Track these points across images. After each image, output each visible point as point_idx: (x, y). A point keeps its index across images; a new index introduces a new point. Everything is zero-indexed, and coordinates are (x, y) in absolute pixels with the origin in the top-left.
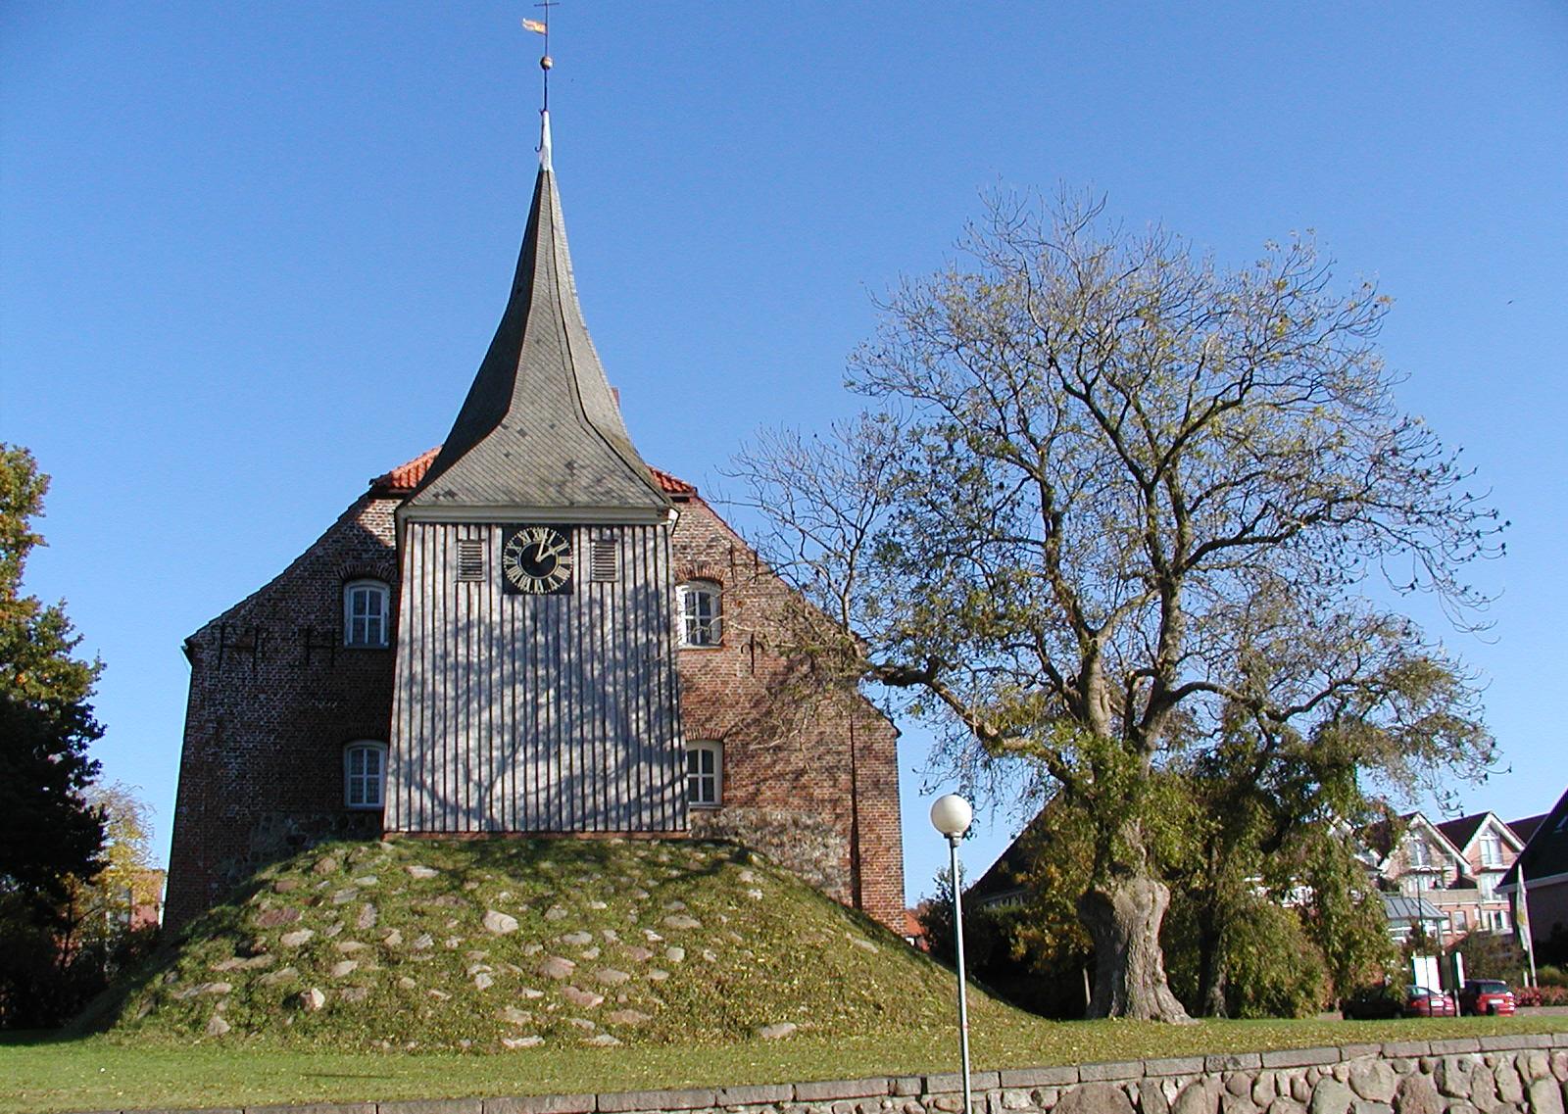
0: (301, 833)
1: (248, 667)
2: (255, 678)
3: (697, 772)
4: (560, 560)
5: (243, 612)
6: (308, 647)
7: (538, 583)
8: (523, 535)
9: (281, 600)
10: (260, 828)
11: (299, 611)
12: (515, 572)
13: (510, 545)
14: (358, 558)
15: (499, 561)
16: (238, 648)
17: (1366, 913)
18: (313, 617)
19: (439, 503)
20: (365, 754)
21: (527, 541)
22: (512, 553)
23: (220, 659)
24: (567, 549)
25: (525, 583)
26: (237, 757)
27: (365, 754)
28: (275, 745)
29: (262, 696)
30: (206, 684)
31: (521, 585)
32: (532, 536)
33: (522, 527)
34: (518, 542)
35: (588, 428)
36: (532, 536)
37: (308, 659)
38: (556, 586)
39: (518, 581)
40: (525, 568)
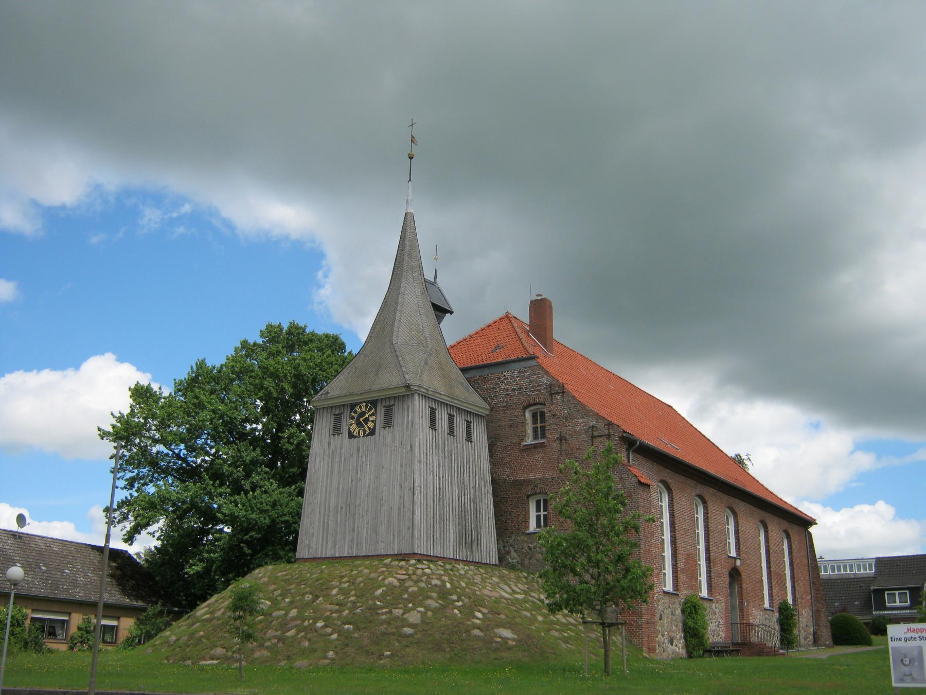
7: (361, 431)
13: (353, 414)
20: (542, 524)
21: (359, 411)
22: (352, 418)
27: (542, 524)
33: (356, 404)
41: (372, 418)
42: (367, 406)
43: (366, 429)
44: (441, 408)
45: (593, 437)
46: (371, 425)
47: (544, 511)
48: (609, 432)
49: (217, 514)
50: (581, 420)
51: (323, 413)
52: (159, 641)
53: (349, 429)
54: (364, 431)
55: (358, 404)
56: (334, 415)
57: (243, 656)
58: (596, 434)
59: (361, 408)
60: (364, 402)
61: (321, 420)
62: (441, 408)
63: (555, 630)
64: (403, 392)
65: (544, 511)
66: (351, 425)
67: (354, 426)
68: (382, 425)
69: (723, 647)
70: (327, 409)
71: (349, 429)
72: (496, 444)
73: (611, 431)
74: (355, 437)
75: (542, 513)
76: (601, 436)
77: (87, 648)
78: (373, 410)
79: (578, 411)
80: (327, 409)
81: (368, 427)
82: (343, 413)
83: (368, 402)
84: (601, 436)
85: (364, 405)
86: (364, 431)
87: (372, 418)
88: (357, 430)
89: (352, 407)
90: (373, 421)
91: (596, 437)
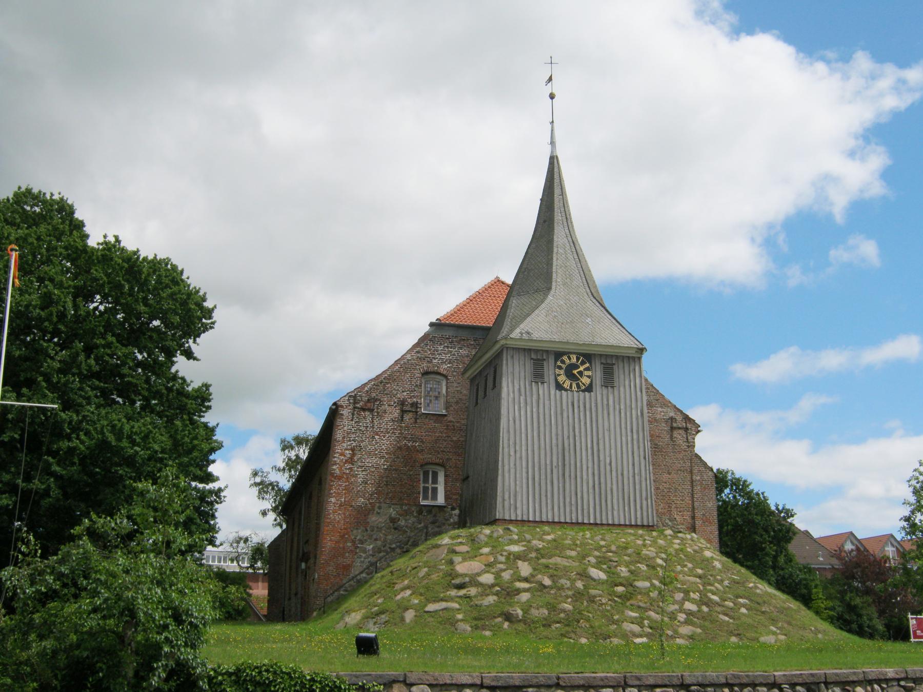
0: (398, 516)
1: (369, 419)
2: (373, 427)
3: (432, 488)
4: (586, 373)
5: (366, 389)
6: (403, 412)
7: (574, 385)
8: (565, 358)
9: (388, 383)
10: (375, 512)
11: (398, 390)
12: (562, 378)
13: (559, 363)
14: (430, 362)
15: (553, 372)
16: (363, 409)
17: (86, 589)
18: (405, 394)
19: (523, 338)
20: (431, 473)
21: (568, 361)
22: (560, 368)
23: (353, 414)
24: (588, 367)
25: (567, 385)
26: (363, 471)
27: (431, 473)
28: (384, 465)
29: (377, 437)
30: (345, 428)
31: (565, 386)
32: (570, 358)
33: (563, 354)
34: (563, 362)
35: (594, 301)
36: (570, 358)
37: (402, 417)
38: (583, 388)
39: (563, 383)
40: (567, 376)
42: (578, 359)
45: (672, 429)
48: (686, 426)
49: (121, 403)
50: (660, 409)
51: (507, 353)
52: (316, 577)
55: (568, 354)
57: (113, 525)
58: (675, 425)
60: (574, 353)
61: (621, 372)
64: (631, 353)
70: (507, 350)
73: (688, 425)
76: (679, 428)
77: (265, 574)
79: (657, 400)
80: (507, 350)
84: (679, 428)
89: (558, 355)
91: (675, 428)
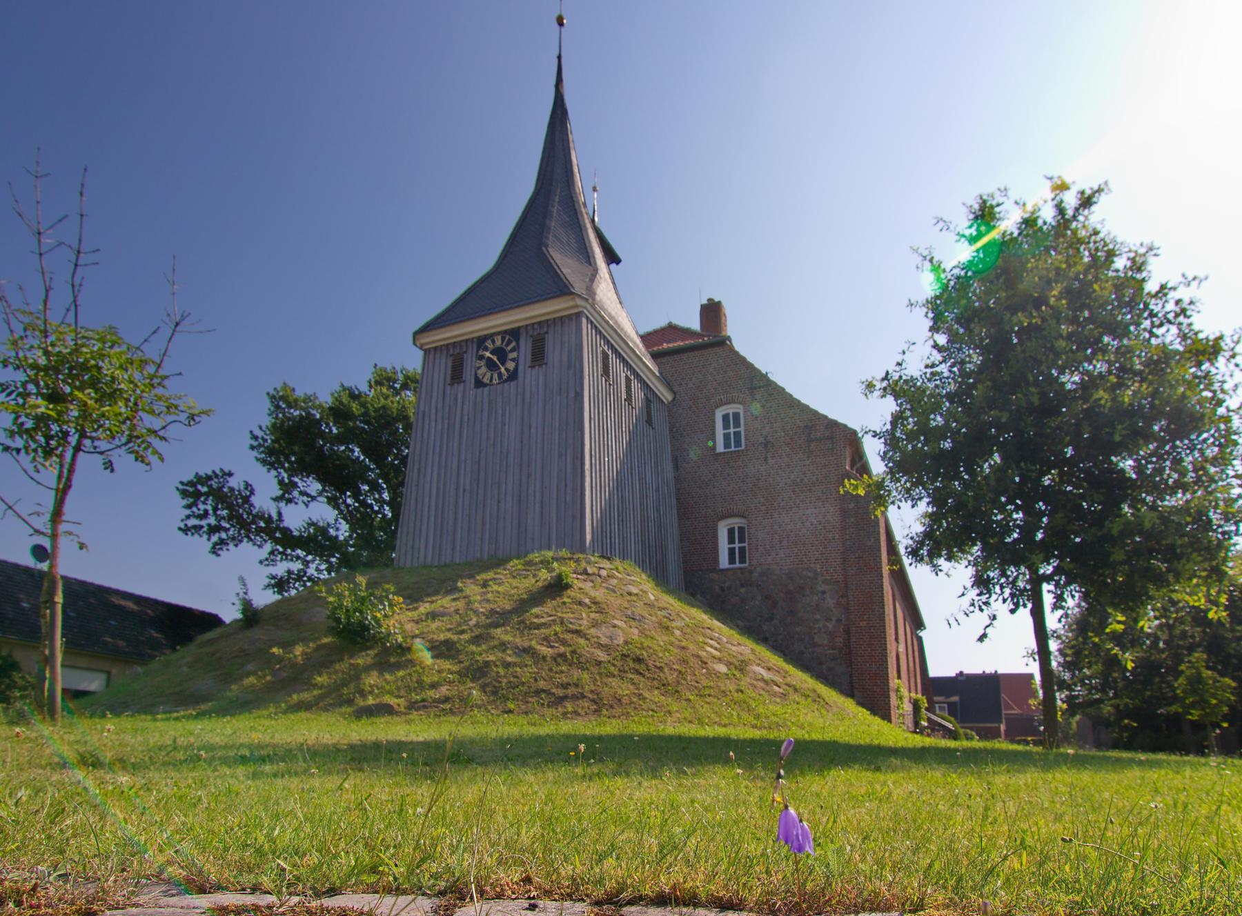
7: (496, 376)
41: (513, 355)
43: (503, 370)
44: (434, 363)
46: (511, 365)
47: (739, 542)
53: (476, 374)
54: (500, 375)
56: (452, 355)
59: (493, 342)
62: (434, 363)
63: (626, 905)
65: (739, 542)
66: (479, 368)
67: (483, 370)
68: (529, 363)
69: (1131, 762)
71: (476, 374)
72: (228, 544)
74: (485, 385)
75: (737, 545)
78: (513, 344)
81: (507, 370)
82: (466, 352)
83: (505, 332)
85: (499, 337)
86: (500, 375)
87: (513, 355)
88: (489, 375)
90: (513, 360)
